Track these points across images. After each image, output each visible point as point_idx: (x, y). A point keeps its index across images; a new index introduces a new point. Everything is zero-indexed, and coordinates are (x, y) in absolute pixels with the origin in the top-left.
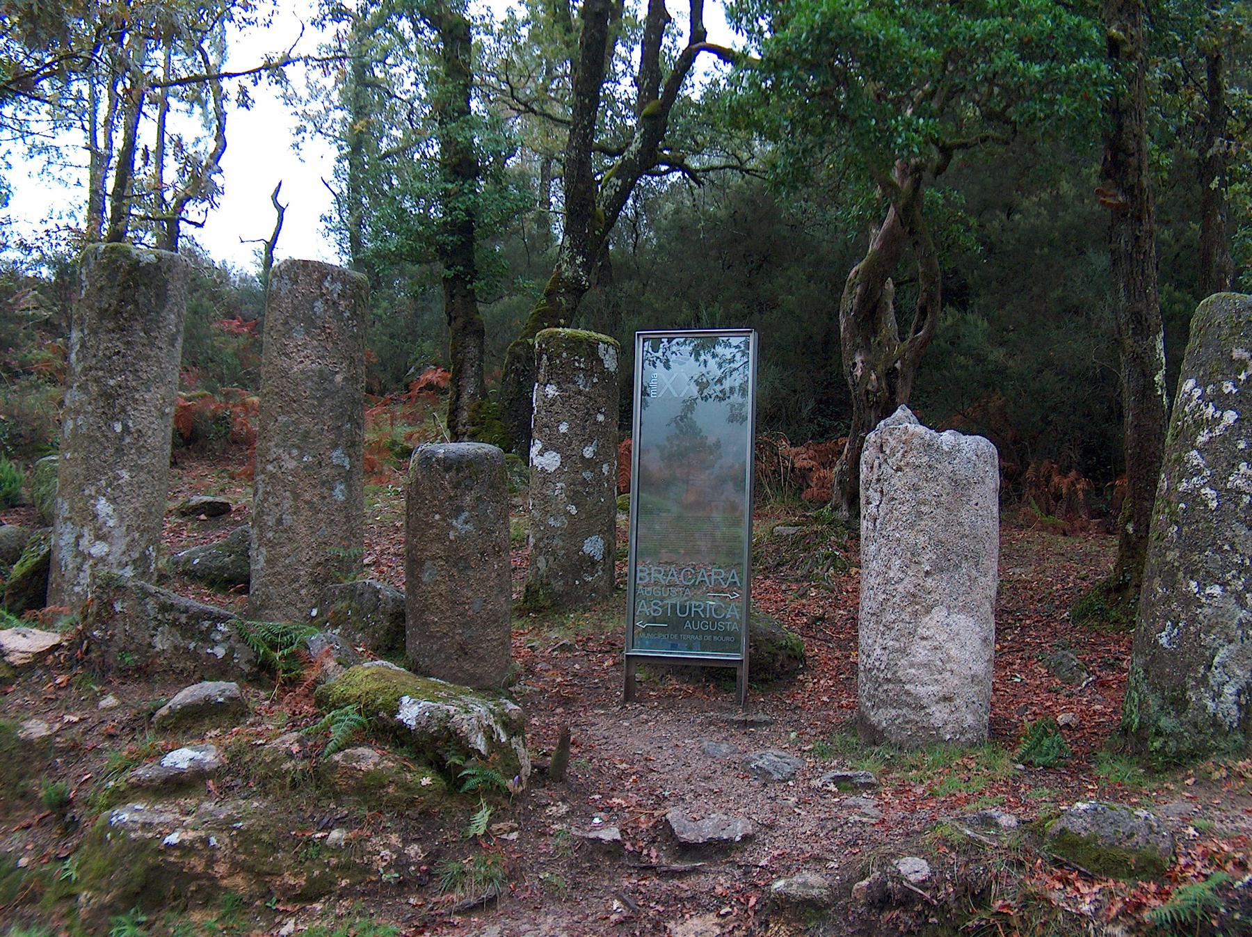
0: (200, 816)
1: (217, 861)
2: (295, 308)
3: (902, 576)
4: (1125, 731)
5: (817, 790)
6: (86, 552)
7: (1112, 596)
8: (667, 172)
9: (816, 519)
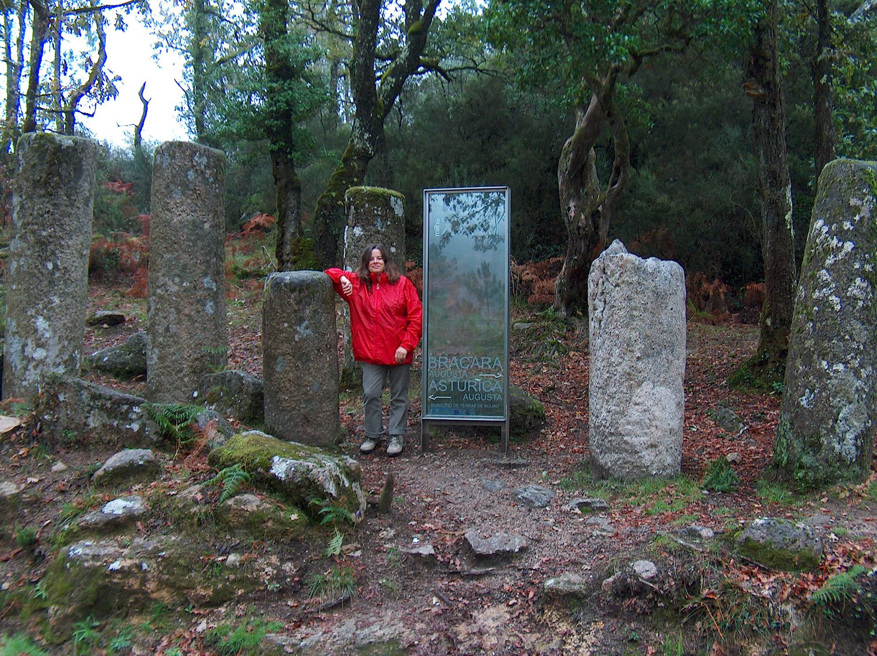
0: (133, 549)
1: (148, 580)
2: (174, 176)
3: (620, 360)
4: (777, 466)
5: (567, 513)
6: (30, 356)
7: (757, 369)
8: (423, 72)
9: (544, 317)
